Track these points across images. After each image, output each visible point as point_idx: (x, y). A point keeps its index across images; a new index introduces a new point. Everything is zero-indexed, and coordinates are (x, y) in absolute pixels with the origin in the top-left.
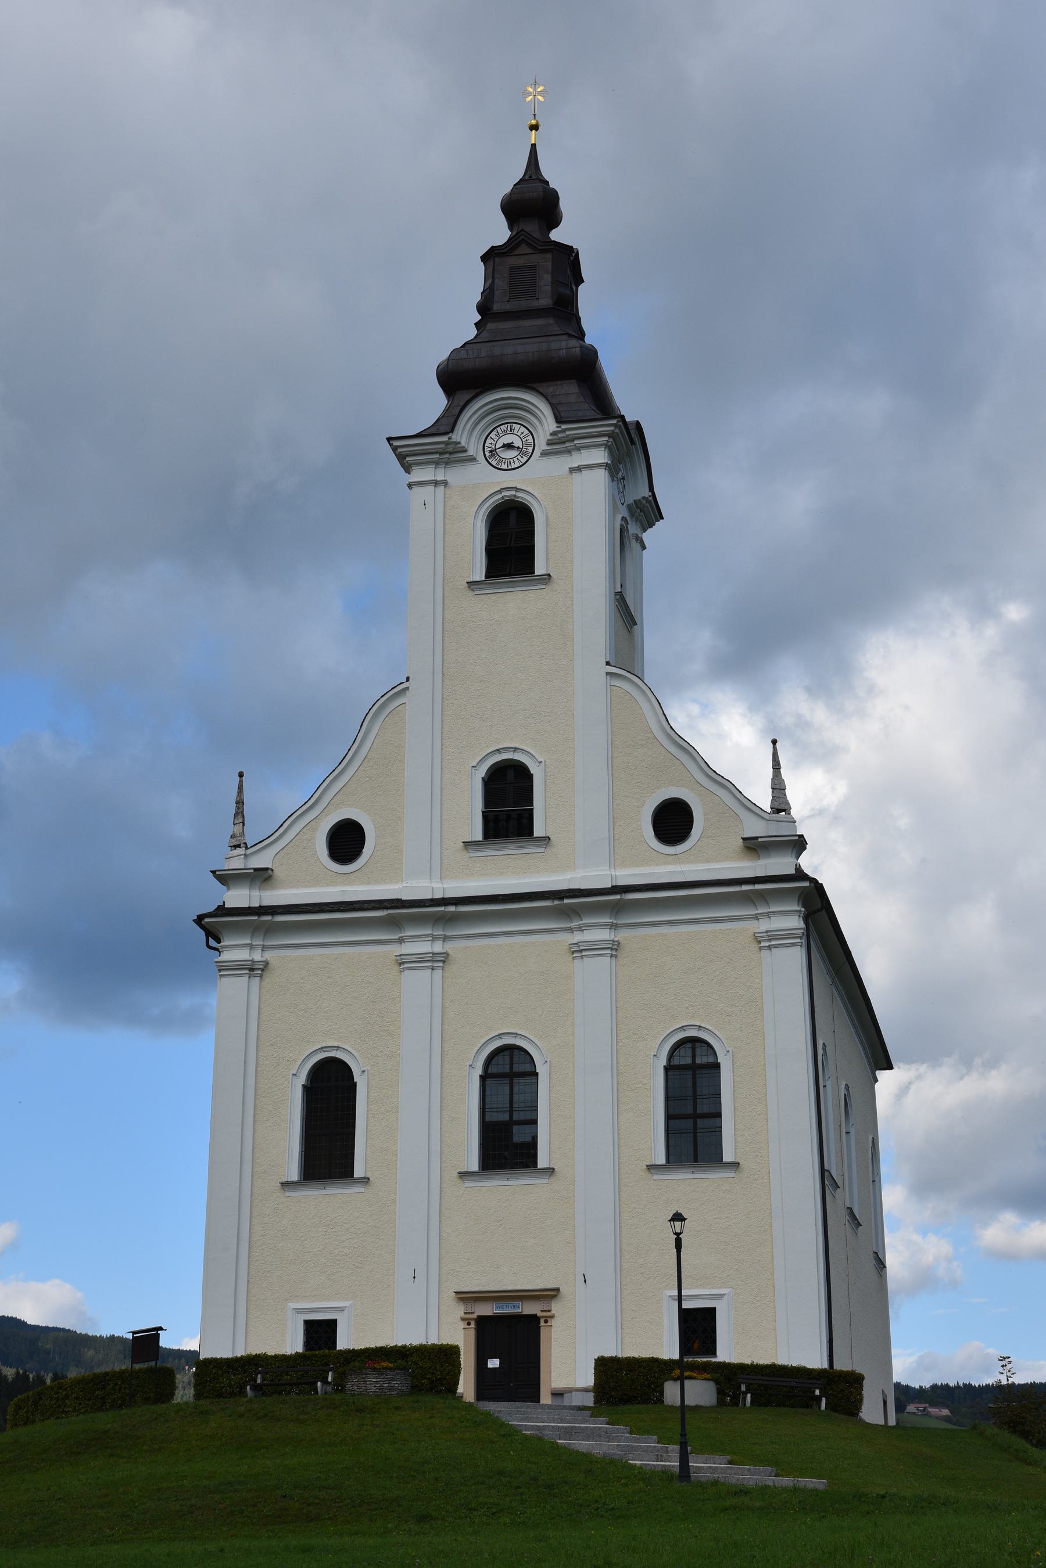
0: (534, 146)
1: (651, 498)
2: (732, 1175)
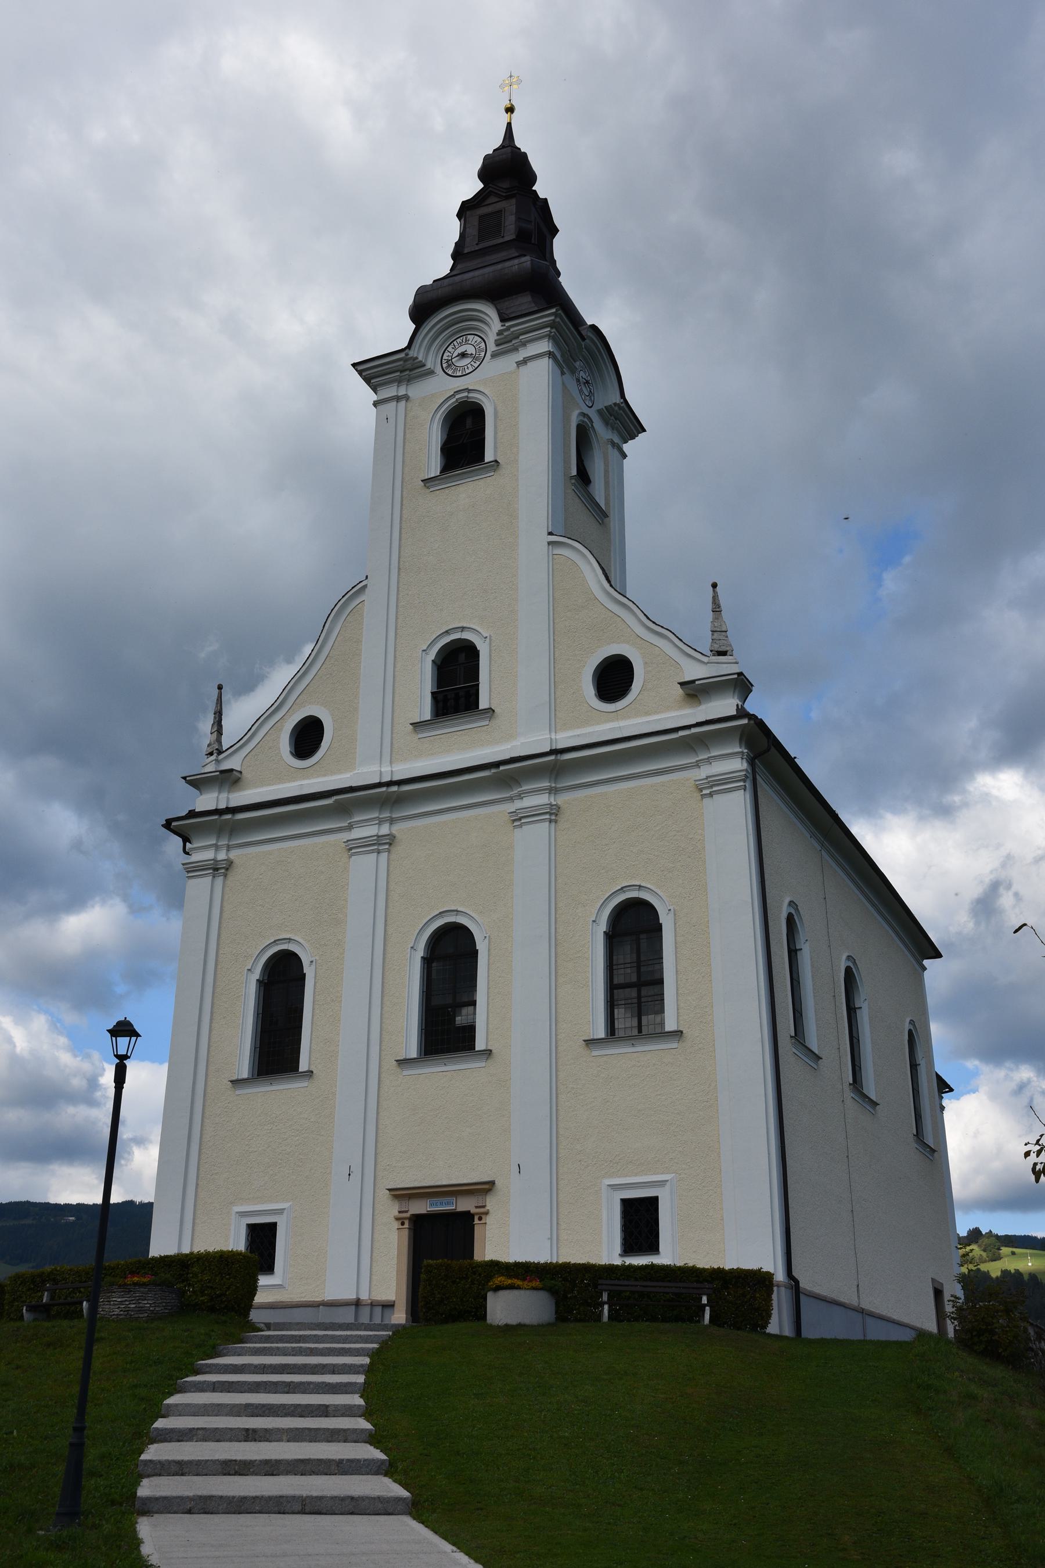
1: (623, 405)
2: (675, 1045)
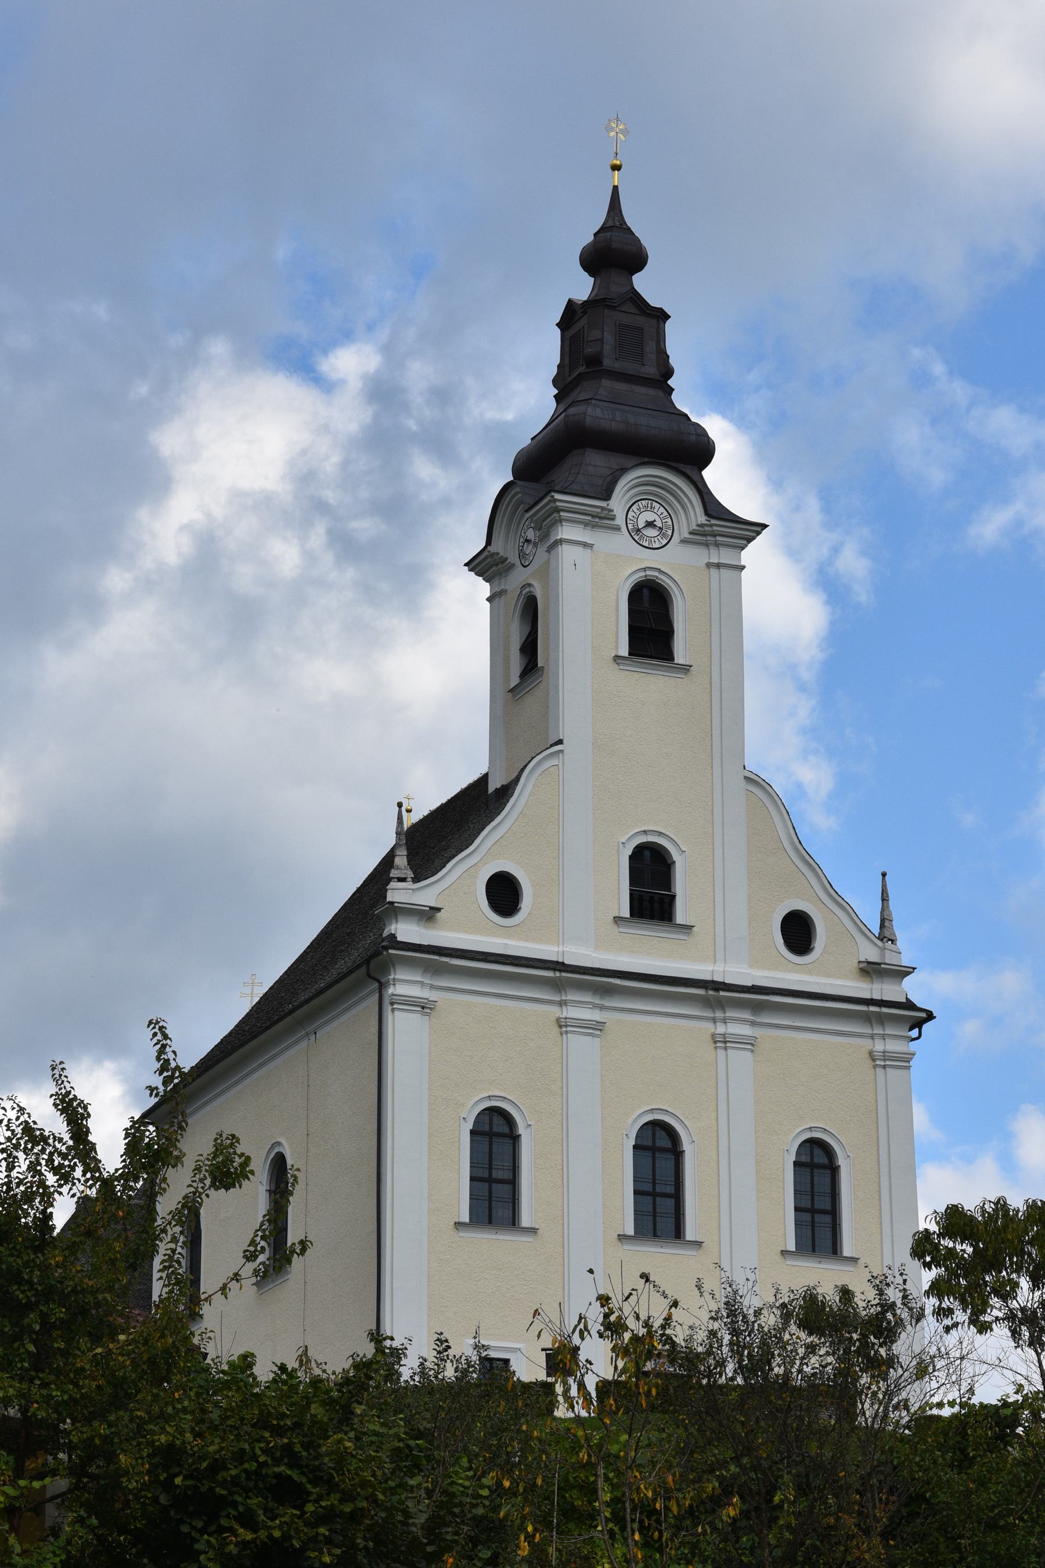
0: (615, 189)
